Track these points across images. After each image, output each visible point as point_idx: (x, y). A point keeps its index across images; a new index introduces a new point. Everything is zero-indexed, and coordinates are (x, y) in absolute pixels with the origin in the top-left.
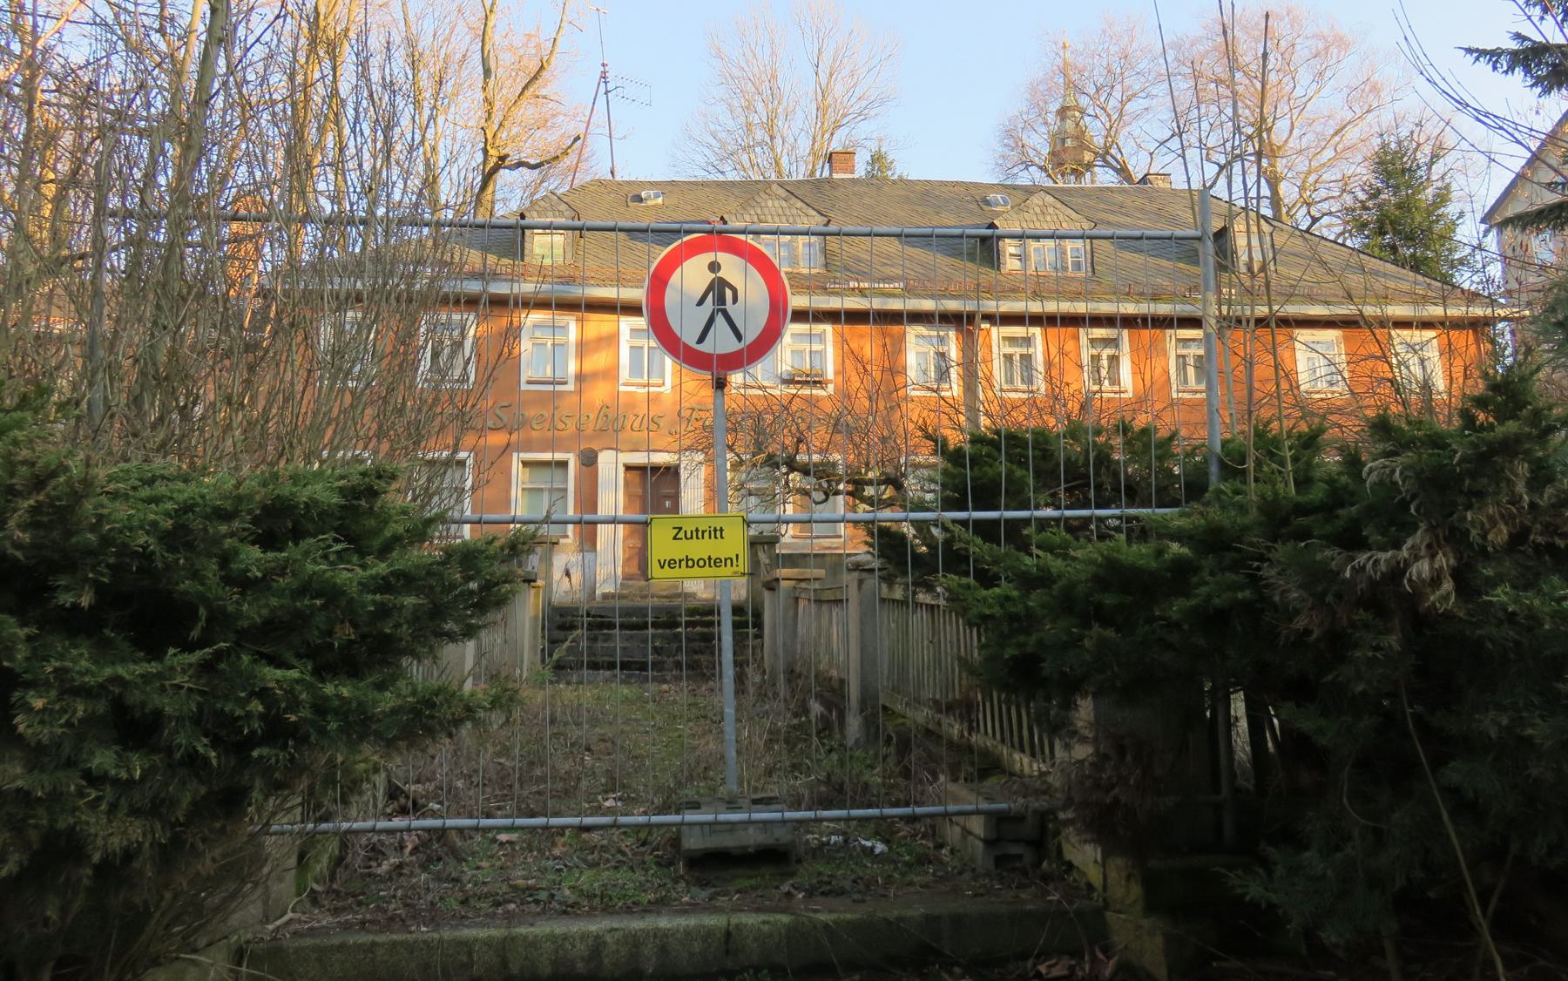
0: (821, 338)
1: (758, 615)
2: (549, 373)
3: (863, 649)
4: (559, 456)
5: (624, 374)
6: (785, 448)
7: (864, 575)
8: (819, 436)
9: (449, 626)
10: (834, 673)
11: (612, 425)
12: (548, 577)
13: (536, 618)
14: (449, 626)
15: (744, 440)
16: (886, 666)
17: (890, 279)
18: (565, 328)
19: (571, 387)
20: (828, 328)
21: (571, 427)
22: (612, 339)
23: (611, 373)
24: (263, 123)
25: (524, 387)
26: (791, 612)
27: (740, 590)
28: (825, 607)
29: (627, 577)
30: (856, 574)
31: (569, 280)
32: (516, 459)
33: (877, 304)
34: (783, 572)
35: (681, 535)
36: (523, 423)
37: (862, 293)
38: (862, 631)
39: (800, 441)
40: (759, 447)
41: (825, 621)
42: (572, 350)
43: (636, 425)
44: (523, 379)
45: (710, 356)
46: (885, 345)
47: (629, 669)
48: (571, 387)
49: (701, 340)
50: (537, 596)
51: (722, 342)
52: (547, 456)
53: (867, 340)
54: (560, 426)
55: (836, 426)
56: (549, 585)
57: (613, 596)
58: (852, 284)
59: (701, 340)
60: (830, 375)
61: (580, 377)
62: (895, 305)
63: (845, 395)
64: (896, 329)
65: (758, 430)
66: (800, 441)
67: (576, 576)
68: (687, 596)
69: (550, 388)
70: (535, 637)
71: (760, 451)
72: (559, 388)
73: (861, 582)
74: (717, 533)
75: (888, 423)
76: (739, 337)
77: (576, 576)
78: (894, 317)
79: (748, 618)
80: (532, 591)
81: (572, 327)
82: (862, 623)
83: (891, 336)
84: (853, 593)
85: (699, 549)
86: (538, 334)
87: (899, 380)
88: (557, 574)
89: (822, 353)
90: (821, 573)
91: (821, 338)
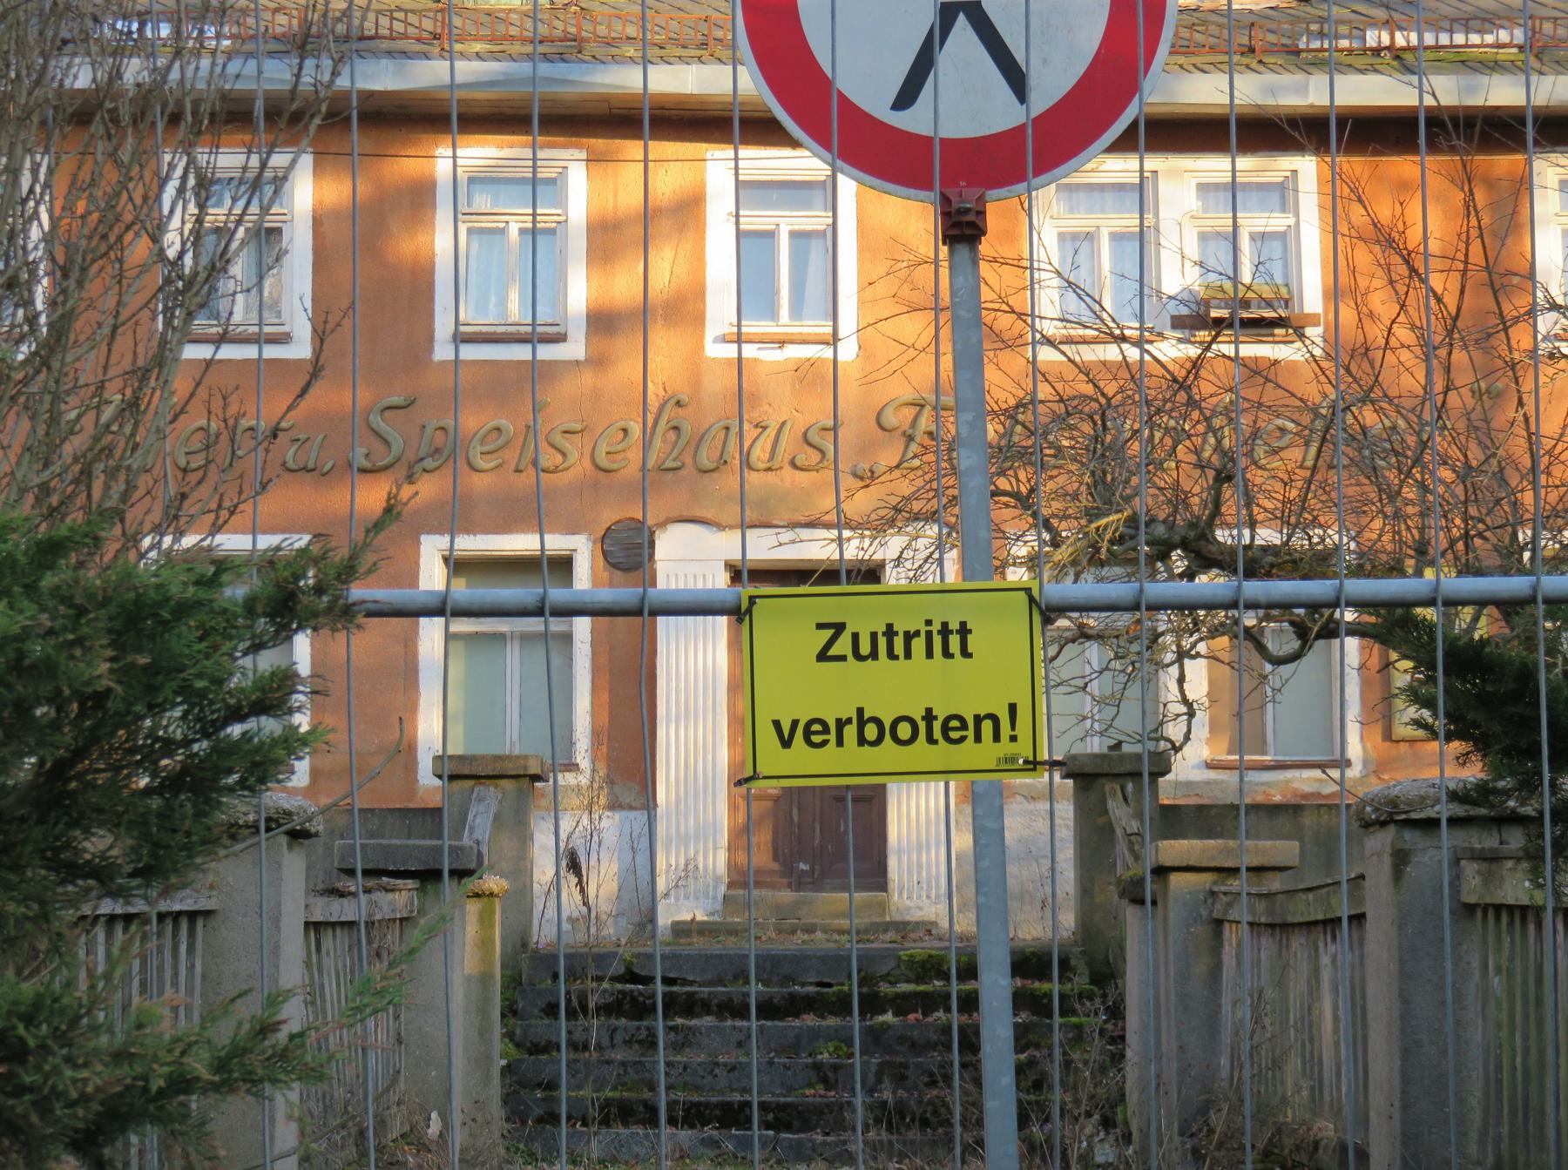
0: (1283, 194)
1: (1106, 975)
2: (515, 309)
3: (1408, 1049)
4: (557, 543)
5: (720, 310)
6: (1179, 498)
7: (1408, 835)
8: (1278, 469)
9: (97, 843)
10: (1326, 1129)
11: (695, 453)
12: (521, 871)
13: (485, 978)
14: (97, 843)
15: (1063, 483)
16: (1475, 1101)
17: (1487, 21)
18: (557, 184)
19: (575, 349)
20: (1306, 167)
21: (578, 465)
22: (690, 208)
23: (686, 308)
24: (100, 158)
25: (443, 351)
26: (1200, 969)
27: (1047, 913)
28: (1298, 942)
29: (740, 878)
30: (1382, 841)
31: (570, 48)
32: (301, 349)
33: (1447, 91)
34: (1175, 850)
35: (843, 646)
36: (446, 452)
37: (1402, 61)
38: (1405, 1000)
39: (1224, 477)
40: (1104, 493)
41: (1297, 985)
42: (578, 243)
43: (759, 454)
44: (443, 327)
45: (922, 144)
46: (1469, 206)
47: (726, 1107)
48: (575, 349)
49: (906, 98)
50: (485, 920)
51: (967, 101)
52: (522, 543)
53: (1423, 199)
54: (549, 458)
55: (1326, 427)
56: (521, 896)
57: (702, 929)
58: (1372, 38)
59: (906, 98)
60: (1312, 299)
61: (602, 322)
62: (1503, 93)
63: (1353, 359)
64: (1503, 163)
65: (1103, 454)
66: (1224, 477)
67: (604, 879)
68: (903, 928)
69: (522, 353)
70: (483, 1032)
71: (1109, 506)
72: (546, 352)
73: (1401, 859)
74: (951, 639)
75: (1481, 429)
76: (1017, 80)
77: (604, 879)
78: (1498, 130)
79: (1069, 985)
80: (473, 907)
81: (581, 184)
82: (1405, 975)
83: (1490, 183)
84: (1379, 900)
85: (895, 688)
86: (482, 201)
87: (1515, 304)
88: (544, 867)
89: (1286, 240)
90: (1284, 850)
91: (1283, 194)
